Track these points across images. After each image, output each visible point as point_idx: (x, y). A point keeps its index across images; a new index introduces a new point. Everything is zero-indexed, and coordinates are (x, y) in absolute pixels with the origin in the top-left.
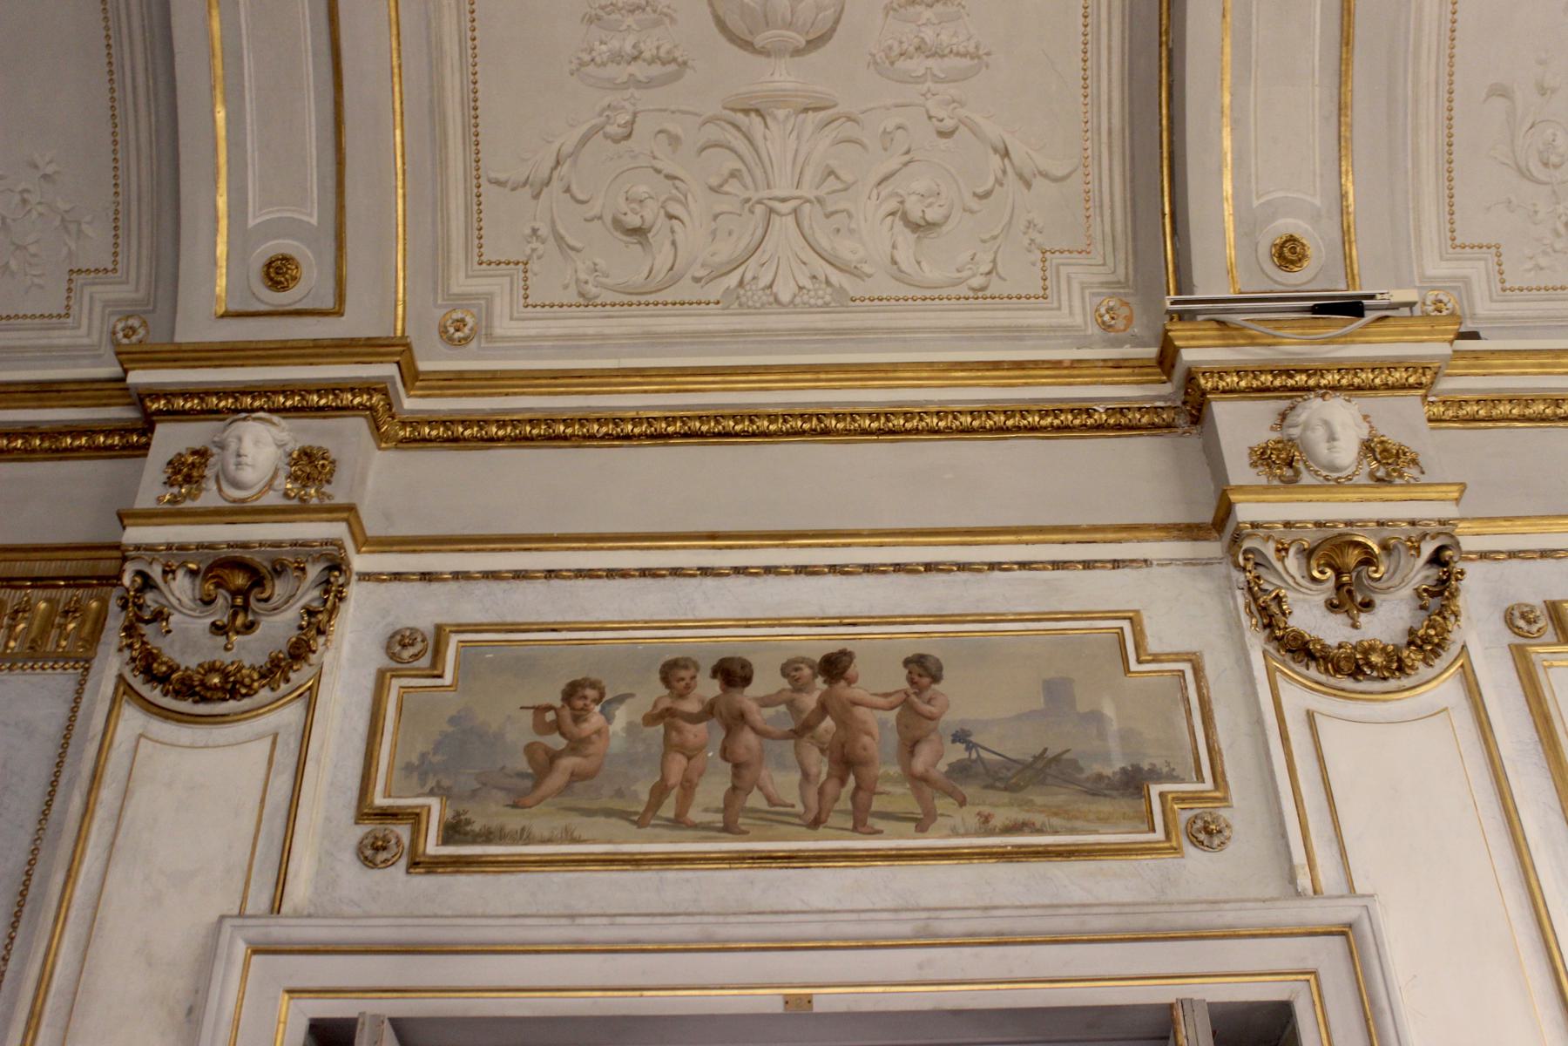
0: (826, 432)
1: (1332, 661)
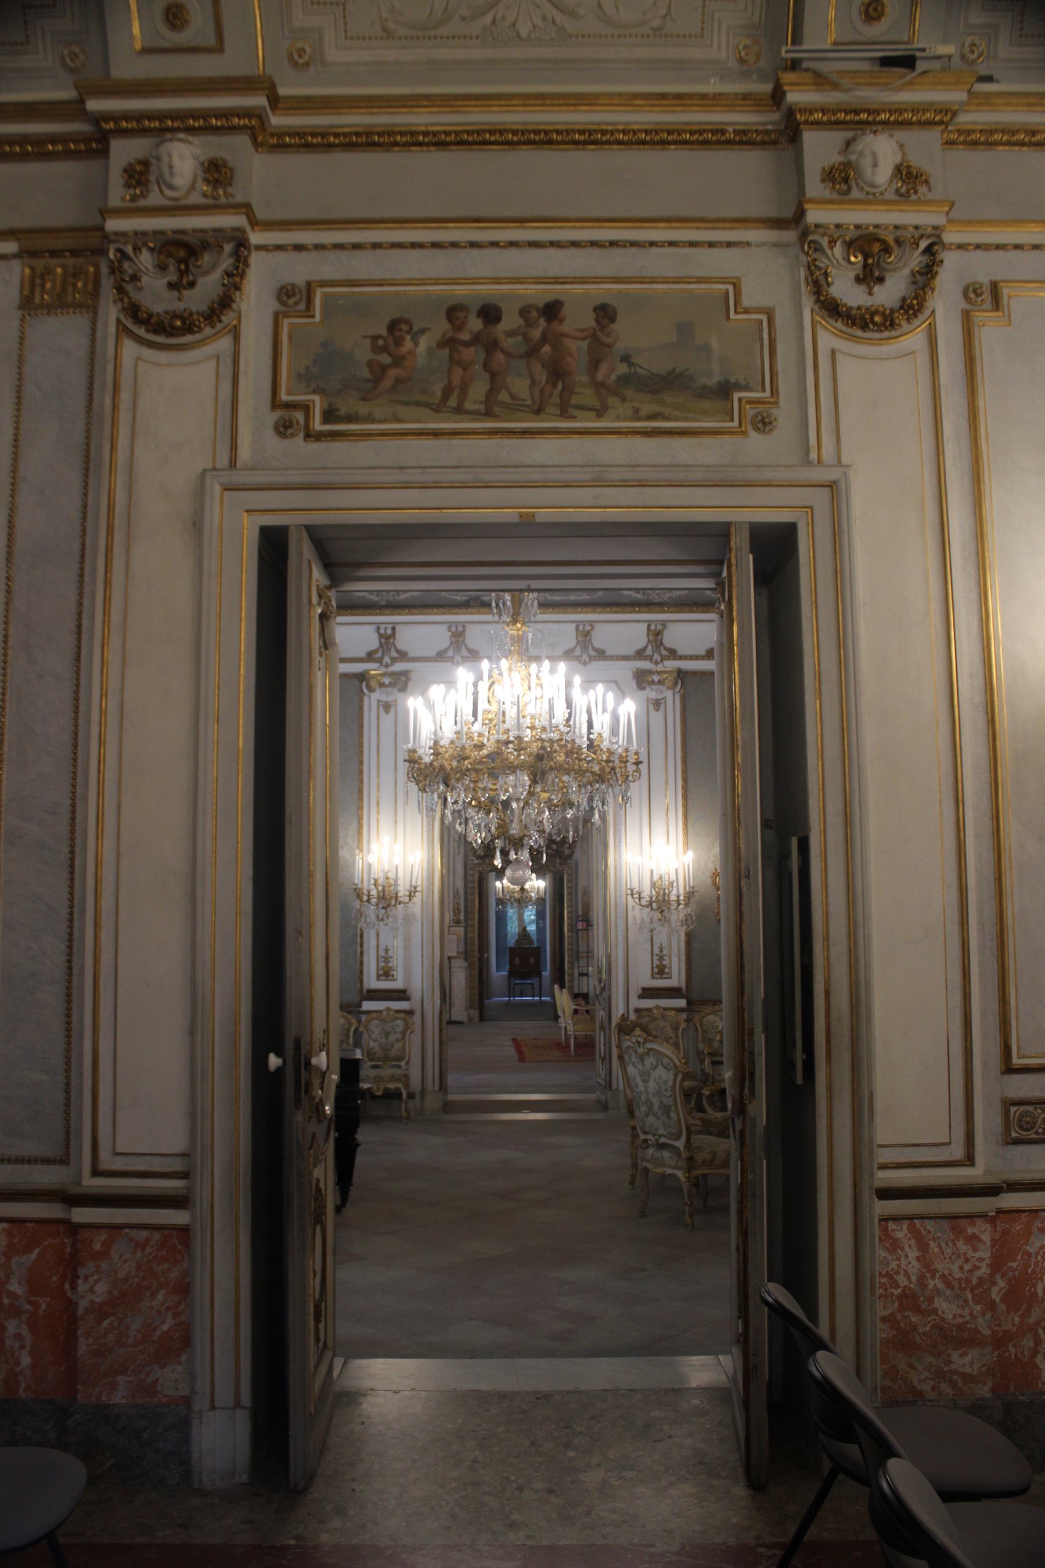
0: (550, 142)
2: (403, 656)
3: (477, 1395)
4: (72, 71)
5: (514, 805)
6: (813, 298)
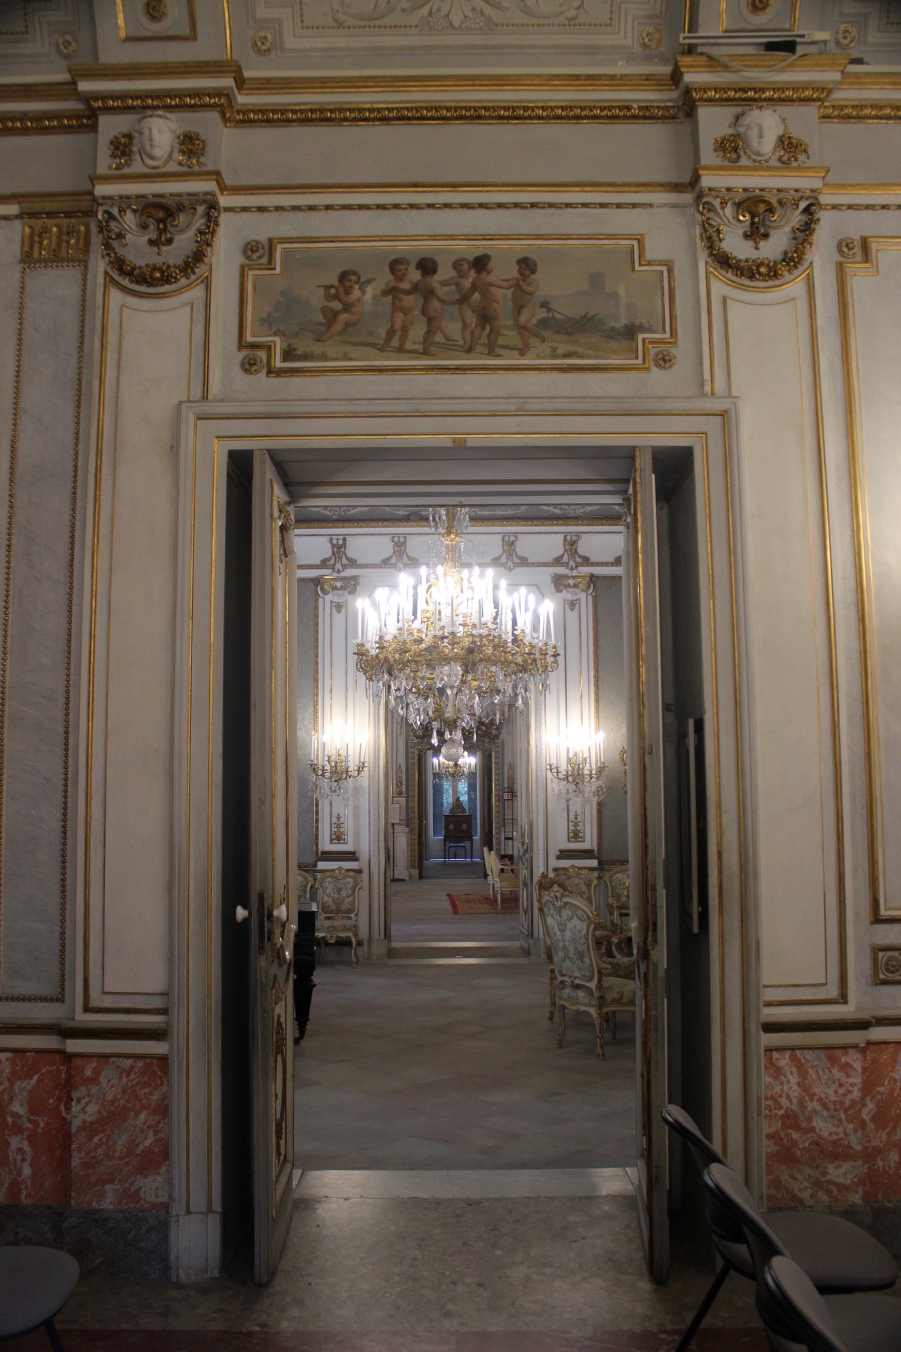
0: (479, 117)
1: (740, 270)
2: (353, 563)
5: (449, 692)
6: (707, 252)
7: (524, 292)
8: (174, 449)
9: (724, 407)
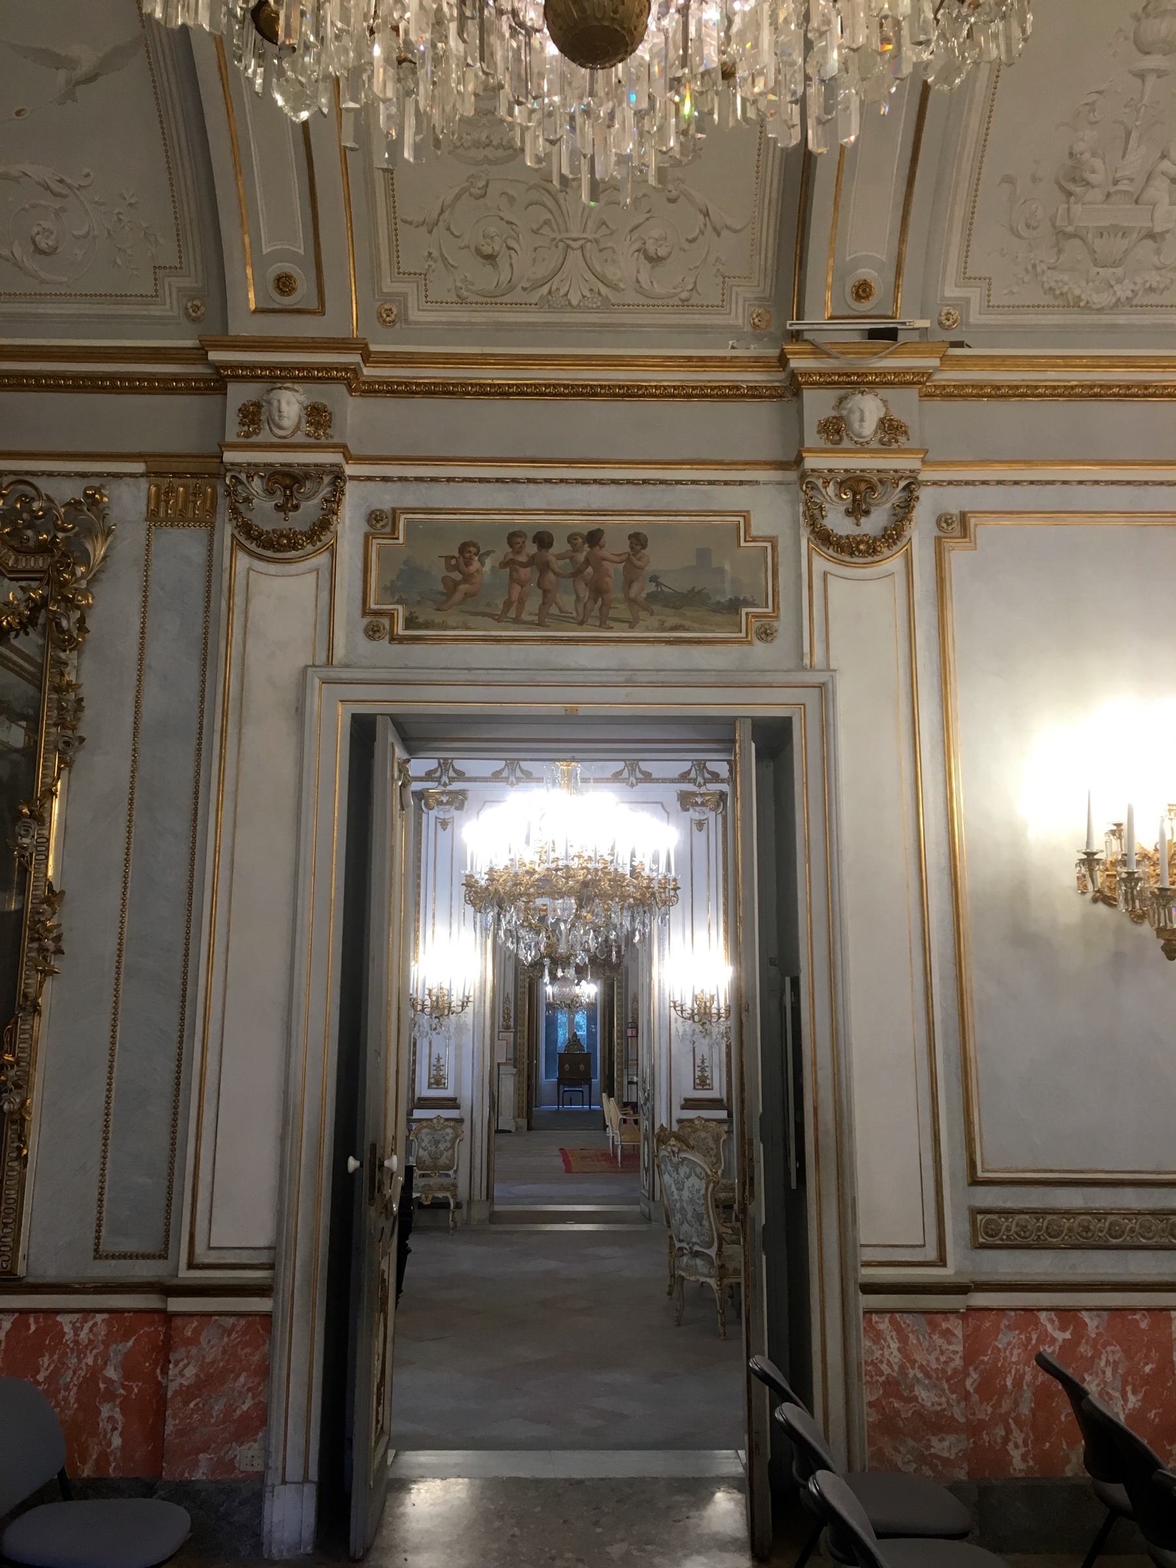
0: (595, 395)
2: (460, 776)
3: (517, 1481)
4: (194, 320)
5: (562, 927)
6: (809, 529)
7: (635, 567)
8: (300, 711)
9: (822, 680)
